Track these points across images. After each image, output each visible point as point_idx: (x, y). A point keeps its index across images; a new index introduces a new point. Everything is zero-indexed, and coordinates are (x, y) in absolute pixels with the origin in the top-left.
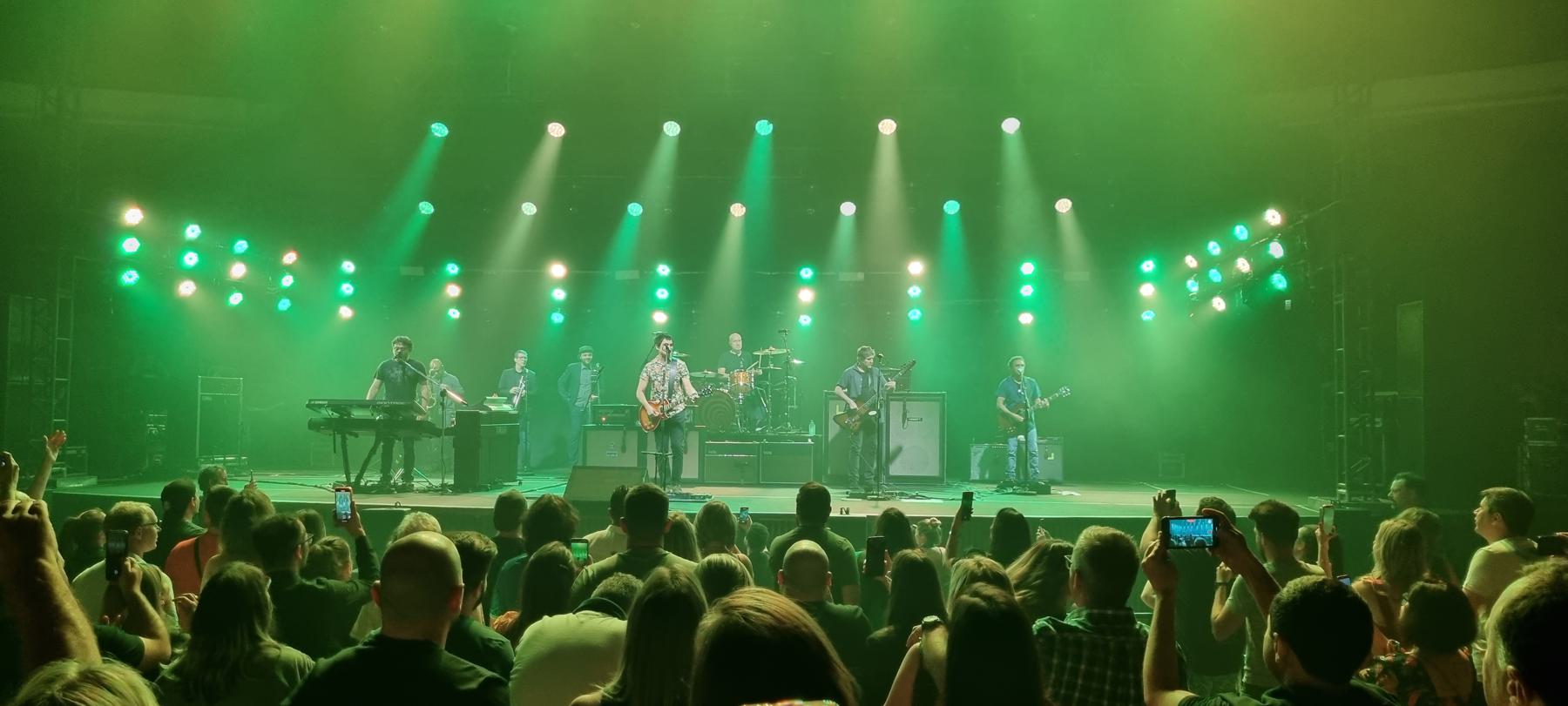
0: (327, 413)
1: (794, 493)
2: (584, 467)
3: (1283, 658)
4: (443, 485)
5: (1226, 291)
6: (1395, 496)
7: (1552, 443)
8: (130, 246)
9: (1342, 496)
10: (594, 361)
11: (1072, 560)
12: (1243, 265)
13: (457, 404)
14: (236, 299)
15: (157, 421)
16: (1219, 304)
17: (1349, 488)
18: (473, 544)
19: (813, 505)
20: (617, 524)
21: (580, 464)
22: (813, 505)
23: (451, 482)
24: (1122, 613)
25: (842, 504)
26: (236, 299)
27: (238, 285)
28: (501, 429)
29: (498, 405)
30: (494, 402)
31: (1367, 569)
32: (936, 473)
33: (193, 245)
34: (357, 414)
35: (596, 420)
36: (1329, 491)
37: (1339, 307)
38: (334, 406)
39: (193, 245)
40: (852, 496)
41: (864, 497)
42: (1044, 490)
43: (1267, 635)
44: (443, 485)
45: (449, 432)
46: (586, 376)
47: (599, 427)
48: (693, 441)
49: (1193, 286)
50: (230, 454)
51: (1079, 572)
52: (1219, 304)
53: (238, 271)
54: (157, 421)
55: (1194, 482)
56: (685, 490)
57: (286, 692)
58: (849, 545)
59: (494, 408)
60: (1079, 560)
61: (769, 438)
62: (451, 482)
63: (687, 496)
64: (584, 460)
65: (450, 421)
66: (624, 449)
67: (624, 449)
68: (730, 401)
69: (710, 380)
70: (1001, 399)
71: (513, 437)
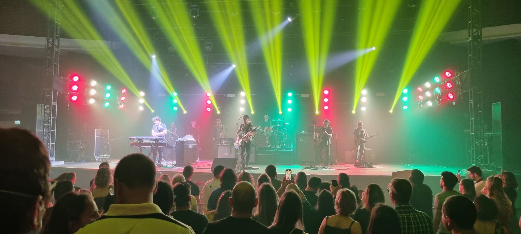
1: (265, 167)
5: (433, 99)
6: (204, 212)
8: (93, 92)
12: (438, 90)
14: (107, 104)
15: (83, 144)
16: (430, 104)
19: (271, 170)
22: (271, 170)
24: (407, 205)
25: (280, 170)
26: (107, 104)
27: (108, 100)
33: (109, 91)
37: (471, 104)
39: (109, 91)
40: (306, 168)
41: (310, 168)
42: (371, 166)
48: (253, 149)
49: (421, 98)
50: (105, 154)
52: (430, 104)
53: (108, 95)
54: (83, 144)
56: (249, 166)
58: (154, 188)
61: (277, 149)
66: (231, 153)
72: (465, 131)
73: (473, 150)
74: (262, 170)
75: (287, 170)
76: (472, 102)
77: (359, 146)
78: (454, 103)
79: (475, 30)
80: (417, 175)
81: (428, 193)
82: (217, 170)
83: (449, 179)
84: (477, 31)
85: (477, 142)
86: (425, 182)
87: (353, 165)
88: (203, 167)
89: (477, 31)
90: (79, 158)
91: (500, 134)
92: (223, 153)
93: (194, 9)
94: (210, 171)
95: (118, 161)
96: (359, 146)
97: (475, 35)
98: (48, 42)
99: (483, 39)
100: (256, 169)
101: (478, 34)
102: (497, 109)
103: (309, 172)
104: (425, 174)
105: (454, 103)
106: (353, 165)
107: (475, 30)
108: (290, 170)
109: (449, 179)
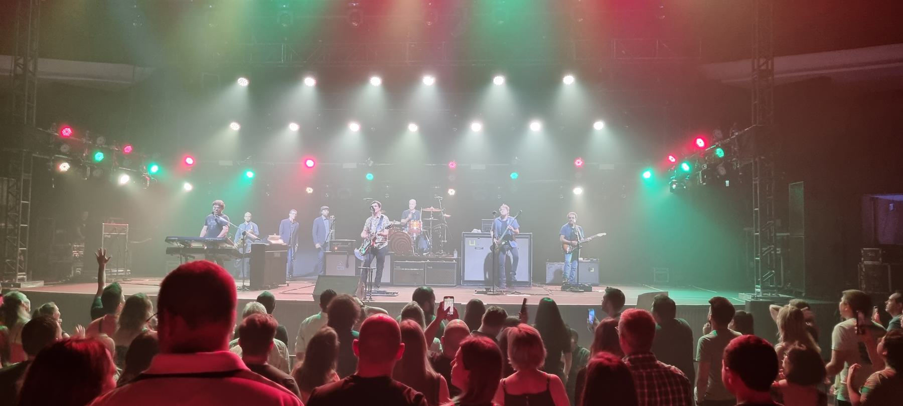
0: (176, 245)
1: (411, 291)
2: (324, 276)
3: (733, 381)
4: (244, 286)
7: (876, 263)
9: (758, 293)
10: (329, 215)
11: (618, 328)
13: (253, 240)
15: (79, 249)
17: (763, 288)
18: (267, 321)
20: (324, 310)
21: (321, 274)
23: (247, 284)
24: (648, 355)
25: (439, 295)
28: (277, 254)
29: (277, 240)
30: (273, 239)
31: (705, 341)
32: (527, 280)
34: (195, 245)
35: (332, 249)
36: (750, 289)
37: (756, 185)
38: (182, 241)
40: (478, 293)
41: (485, 293)
43: (723, 370)
44: (244, 286)
45: (248, 255)
46: (327, 224)
47: (333, 252)
48: (387, 261)
51: (622, 335)
55: (633, 282)
56: (381, 289)
57: (882, 332)
59: (273, 242)
60: (622, 328)
62: (247, 284)
63: (384, 292)
64: (325, 272)
65: (249, 250)
66: (347, 266)
67: (347, 266)
68: (409, 238)
69: (397, 226)
70: (563, 236)
71: (283, 259)
72: (745, 229)
73: (757, 261)
74: (405, 296)
75: (446, 298)
76: (756, 181)
77: (480, 231)
78: (727, 182)
79: (762, 61)
80: (665, 306)
81: (685, 335)
82: (326, 299)
83: (721, 311)
84: (766, 63)
85: (764, 249)
86: (680, 318)
87: (559, 288)
88: (299, 291)
89: (766, 63)
90: (72, 275)
91: (801, 234)
92: (341, 269)
93: (285, 12)
94: (311, 299)
95: (163, 279)
96: (480, 231)
97: (763, 68)
98: (17, 65)
99: (776, 76)
100: (393, 294)
101: (767, 66)
102: (797, 192)
103: (488, 301)
104: (276, 298)
105: (727, 182)
106: (559, 288)
107: (762, 61)
108: (452, 297)
109: (721, 311)
